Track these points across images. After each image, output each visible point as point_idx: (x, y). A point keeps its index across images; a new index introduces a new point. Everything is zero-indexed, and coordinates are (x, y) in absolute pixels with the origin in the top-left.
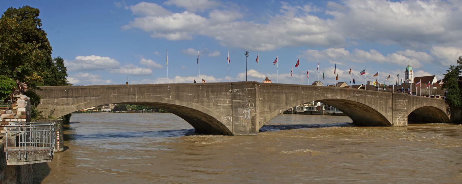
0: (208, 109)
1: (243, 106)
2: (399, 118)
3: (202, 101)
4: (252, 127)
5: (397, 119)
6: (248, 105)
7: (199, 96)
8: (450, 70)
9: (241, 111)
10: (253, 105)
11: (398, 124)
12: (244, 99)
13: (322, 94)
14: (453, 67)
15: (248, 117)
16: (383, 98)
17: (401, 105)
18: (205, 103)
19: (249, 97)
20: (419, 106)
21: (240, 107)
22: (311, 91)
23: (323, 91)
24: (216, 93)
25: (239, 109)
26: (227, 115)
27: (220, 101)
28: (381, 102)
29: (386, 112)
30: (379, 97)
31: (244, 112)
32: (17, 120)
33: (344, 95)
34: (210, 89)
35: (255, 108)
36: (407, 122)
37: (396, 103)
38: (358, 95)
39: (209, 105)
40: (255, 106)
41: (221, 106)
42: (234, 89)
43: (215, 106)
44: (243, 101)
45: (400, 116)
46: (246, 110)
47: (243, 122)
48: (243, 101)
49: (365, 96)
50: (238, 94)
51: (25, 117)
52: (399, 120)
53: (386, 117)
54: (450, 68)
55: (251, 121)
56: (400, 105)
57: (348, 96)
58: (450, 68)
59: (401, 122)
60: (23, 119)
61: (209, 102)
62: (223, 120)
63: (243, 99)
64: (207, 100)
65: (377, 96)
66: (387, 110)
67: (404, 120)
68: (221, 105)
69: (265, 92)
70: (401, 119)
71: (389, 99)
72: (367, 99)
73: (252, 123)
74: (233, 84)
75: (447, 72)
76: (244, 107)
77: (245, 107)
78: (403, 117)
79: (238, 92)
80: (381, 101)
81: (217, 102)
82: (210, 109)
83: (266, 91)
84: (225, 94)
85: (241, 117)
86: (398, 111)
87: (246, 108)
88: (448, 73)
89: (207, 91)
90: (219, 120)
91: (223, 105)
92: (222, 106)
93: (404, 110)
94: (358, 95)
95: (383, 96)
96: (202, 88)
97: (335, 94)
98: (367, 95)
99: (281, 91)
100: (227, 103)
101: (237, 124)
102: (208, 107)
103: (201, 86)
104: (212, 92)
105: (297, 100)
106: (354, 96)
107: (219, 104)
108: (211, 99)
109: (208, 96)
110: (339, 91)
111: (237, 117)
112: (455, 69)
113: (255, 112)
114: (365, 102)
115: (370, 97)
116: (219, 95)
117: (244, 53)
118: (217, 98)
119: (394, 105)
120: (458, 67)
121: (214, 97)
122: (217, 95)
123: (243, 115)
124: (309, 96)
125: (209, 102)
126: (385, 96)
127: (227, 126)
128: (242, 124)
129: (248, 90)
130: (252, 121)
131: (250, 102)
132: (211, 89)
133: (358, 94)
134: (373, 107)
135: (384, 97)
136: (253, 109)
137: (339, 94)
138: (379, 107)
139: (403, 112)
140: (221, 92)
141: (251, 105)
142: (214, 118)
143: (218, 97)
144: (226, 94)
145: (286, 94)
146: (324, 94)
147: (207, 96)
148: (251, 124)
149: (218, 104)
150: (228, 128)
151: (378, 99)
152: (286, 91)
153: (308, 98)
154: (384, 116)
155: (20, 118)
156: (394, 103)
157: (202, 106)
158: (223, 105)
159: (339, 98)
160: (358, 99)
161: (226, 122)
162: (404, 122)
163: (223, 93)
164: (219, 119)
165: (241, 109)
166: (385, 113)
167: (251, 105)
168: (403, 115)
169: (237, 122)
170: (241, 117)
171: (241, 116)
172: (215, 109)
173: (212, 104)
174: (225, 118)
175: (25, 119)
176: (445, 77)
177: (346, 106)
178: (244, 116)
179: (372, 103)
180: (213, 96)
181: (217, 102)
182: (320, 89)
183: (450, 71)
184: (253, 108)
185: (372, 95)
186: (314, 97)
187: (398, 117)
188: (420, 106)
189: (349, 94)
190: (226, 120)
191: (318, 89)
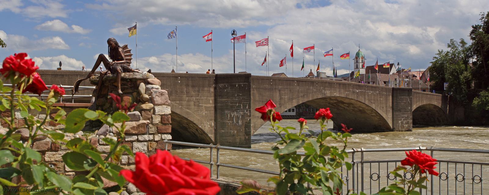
0: (187, 111)
1: (232, 107)
2: (401, 120)
3: (181, 100)
4: (245, 138)
5: (400, 122)
6: (239, 106)
7: (178, 92)
8: (437, 56)
9: (229, 115)
10: (247, 107)
11: (400, 128)
12: (233, 98)
13: (320, 90)
14: (441, 52)
15: (238, 123)
16: (383, 95)
17: (404, 103)
18: (184, 103)
19: (241, 96)
20: (419, 103)
21: (227, 109)
22: (307, 87)
23: (320, 87)
24: (197, 89)
25: (226, 112)
26: (210, 120)
27: (203, 99)
28: (382, 99)
29: (386, 114)
30: (379, 94)
31: (233, 116)
32: (151, 137)
33: (342, 91)
34: (190, 83)
35: (250, 111)
36: (412, 125)
37: (397, 100)
38: (357, 91)
39: (189, 105)
40: (250, 107)
41: (203, 107)
42: (221, 83)
43: (196, 107)
44: (233, 100)
45: (403, 117)
46: (235, 113)
47: (231, 130)
48: (233, 100)
49: (365, 92)
50: (226, 90)
51: (170, 131)
52: (402, 123)
53: (386, 119)
54: (438, 54)
55: (244, 129)
56: (403, 104)
57: (347, 93)
58: (438, 54)
59: (405, 125)
60: (166, 135)
61: (188, 101)
62: (205, 126)
63: (232, 98)
64: (187, 98)
65: (377, 91)
66: (388, 110)
67: (407, 123)
68: (204, 105)
69: (255, 88)
70: (404, 122)
71: (389, 95)
72: (366, 96)
73: (245, 132)
74: (218, 76)
75: (433, 59)
76: (232, 109)
77: (234, 109)
78: (407, 118)
79: (225, 88)
80: (380, 98)
81: (198, 102)
82: (190, 111)
83: (256, 87)
84: (208, 90)
85: (228, 122)
86: (401, 111)
87: (236, 110)
88: (434, 60)
89: (187, 85)
90: (200, 127)
91: (205, 105)
92: (205, 106)
93: (407, 110)
94: (357, 91)
95: (383, 91)
96: (180, 80)
97: (333, 90)
98: (367, 90)
99: (274, 87)
100: (211, 104)
101: (223, 133)
102: (188, 108)
103: (179, 78)
104: (193, 86)
105: (292, 99)
106: (354, 92)
107: (201, 104)
108: (192, 97)
109: (189, 92)
110: (338, 85)
111: (224, 123)
112: (444, 55)
113: (250, 116)
114: (365, 99)
115: (370, 93)
116: (201, 92)
117: (230, 32)
118: (198, 95)
119: (395, 103)
120: (448, 52)
121: (195, 93)
122: (199, 91)
123: (232, 119)
124: (305, 94)
125: (188, 101)
126: (385, 92)
127: (210, 135)
128: (230, 133)
129: (239, 85)
130: (245, 130)
131: (242, 102)
132: (192, 82)
133: (357, 89)
134: (373, 106)
135: (384, 93)
136: (247, 112)
137: (338, 90)
138: (379, 106)
139: (406, 112)
140: (203, 87)
141: (244, 107)
142: (194, 124)
143: (200, 94)
144: (210, 90)
145: (280, 91)
146: (322, 90)
147: (186, 92)
148: (244, 133)
149: (199, 104)
150: (211, 137)
151: (379, 95)
152: (280, 87)
153: (304, 96)
154: (384, 118)
155: (159, 133)
156: (395, 101)
157: (180, 107)
158: (205, 105)
159: (338, 95)
160: (357, 97)
161: (208, 130)
162: (408, 126)
163: (206, 89)
164: (200, 125)
165: (229, 112)
166: (385, 114)
167: (244, 107)
168: (406, 116)
169: (222, 129)
170: (228, 123)
171: (229, 121)
172: (196, 111)
173: (192, 103)
174: (207, 124)
175: (170, 134)
176: (433, 65)
177: (335, 106)
178: (233, 120)
179: (372, 101)
180: (194, 92)
181: (198, 102)
182: (317, 84)
183: (439, 58)
184: (247, 111)
185: (372, 91)
186: (311, 95)
187: (400, 119)
188: (420, 105)
189: (348, 90)
190: (209, 126)
191: (315, 84)
